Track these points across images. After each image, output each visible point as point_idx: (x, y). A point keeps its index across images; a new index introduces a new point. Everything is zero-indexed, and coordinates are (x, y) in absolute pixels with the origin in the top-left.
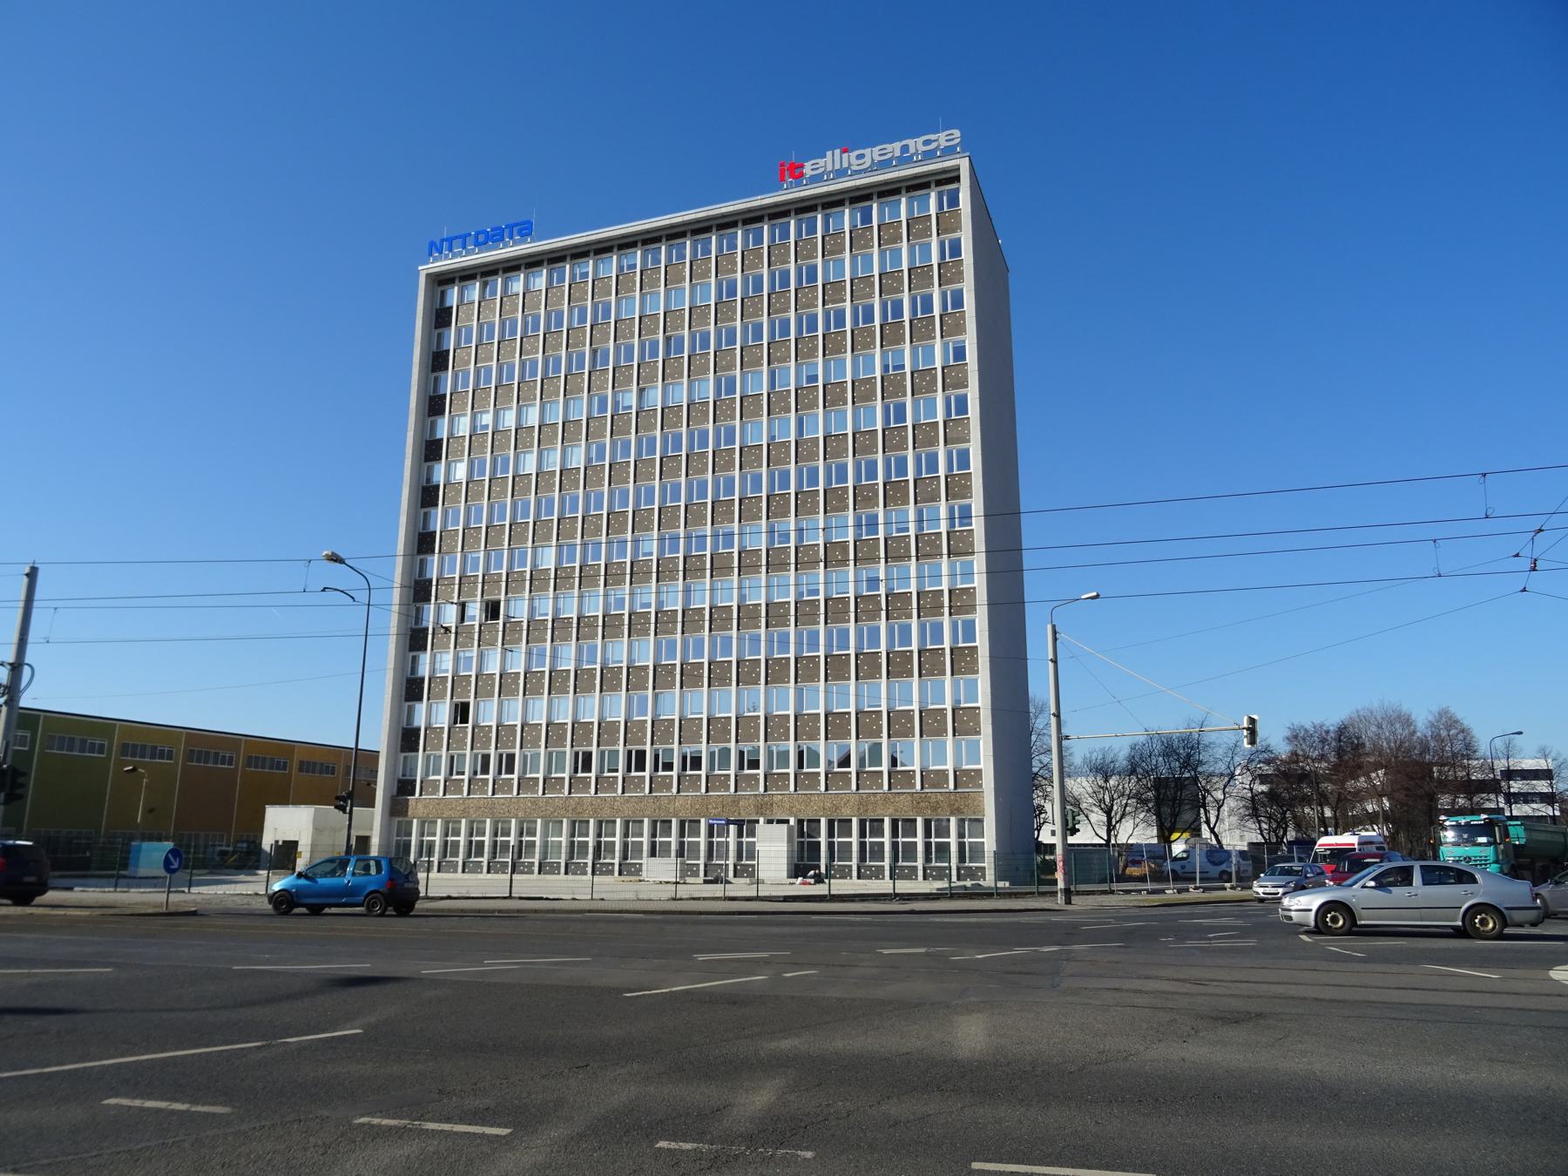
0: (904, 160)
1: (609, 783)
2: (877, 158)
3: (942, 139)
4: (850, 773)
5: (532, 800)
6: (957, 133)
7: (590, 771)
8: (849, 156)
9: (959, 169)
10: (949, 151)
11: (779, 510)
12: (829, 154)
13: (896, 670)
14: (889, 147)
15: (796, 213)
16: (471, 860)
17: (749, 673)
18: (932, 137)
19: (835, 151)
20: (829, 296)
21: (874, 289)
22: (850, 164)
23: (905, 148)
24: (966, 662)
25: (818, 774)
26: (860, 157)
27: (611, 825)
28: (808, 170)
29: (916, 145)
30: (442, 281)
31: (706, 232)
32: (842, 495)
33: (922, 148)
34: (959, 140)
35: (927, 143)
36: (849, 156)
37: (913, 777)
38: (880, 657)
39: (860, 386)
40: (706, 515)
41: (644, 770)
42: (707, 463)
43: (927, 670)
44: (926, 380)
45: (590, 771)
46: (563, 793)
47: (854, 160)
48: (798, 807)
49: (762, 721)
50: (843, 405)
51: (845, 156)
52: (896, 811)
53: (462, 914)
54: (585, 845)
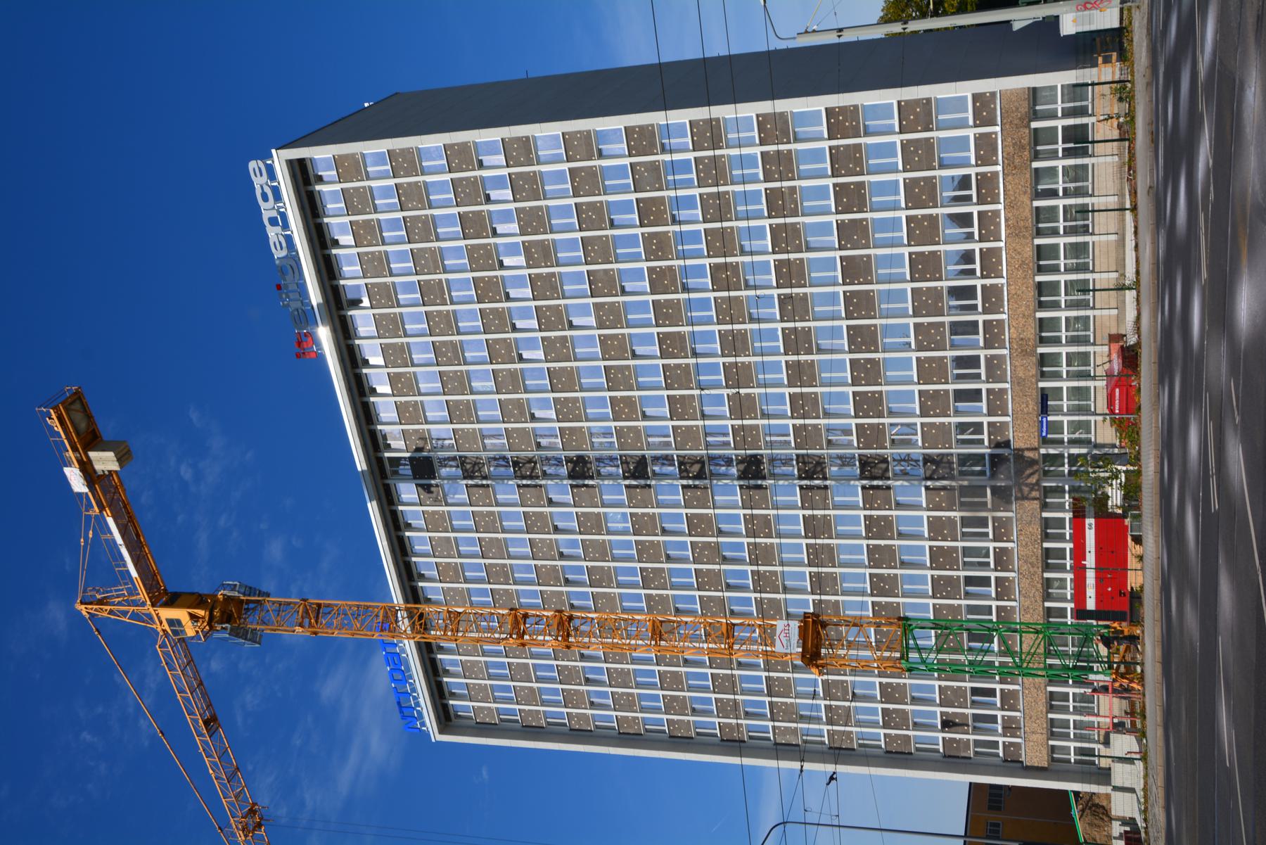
1: (1000, 527)
3: (259, 181)
5: (1022, 612)
6: (252, 165)
7: (989, 578)
10: (272, 175)
13: (857, 202)
15: (342, 308)
16: (1093, 440)
17: (867, 371)
20: (436, 298)
21: (426, 248)
23: (273, 222)
24: (845, 120)
25: (1002, 690)
29: (267, 210)
30: (446, 719)
31: (376, 437)
32: (656, 273)
34: (259, 162)
35: (265, 198)
37: (984, 175)
38: (843, 221)
40: (687, 427)
41: (977, 322)
42: (628, 428)
43: (855, 166)
45: (989, 578)
46: (1014, 578)
48: (1023, 308)
50: (555, 277)
52: (1025, 193)
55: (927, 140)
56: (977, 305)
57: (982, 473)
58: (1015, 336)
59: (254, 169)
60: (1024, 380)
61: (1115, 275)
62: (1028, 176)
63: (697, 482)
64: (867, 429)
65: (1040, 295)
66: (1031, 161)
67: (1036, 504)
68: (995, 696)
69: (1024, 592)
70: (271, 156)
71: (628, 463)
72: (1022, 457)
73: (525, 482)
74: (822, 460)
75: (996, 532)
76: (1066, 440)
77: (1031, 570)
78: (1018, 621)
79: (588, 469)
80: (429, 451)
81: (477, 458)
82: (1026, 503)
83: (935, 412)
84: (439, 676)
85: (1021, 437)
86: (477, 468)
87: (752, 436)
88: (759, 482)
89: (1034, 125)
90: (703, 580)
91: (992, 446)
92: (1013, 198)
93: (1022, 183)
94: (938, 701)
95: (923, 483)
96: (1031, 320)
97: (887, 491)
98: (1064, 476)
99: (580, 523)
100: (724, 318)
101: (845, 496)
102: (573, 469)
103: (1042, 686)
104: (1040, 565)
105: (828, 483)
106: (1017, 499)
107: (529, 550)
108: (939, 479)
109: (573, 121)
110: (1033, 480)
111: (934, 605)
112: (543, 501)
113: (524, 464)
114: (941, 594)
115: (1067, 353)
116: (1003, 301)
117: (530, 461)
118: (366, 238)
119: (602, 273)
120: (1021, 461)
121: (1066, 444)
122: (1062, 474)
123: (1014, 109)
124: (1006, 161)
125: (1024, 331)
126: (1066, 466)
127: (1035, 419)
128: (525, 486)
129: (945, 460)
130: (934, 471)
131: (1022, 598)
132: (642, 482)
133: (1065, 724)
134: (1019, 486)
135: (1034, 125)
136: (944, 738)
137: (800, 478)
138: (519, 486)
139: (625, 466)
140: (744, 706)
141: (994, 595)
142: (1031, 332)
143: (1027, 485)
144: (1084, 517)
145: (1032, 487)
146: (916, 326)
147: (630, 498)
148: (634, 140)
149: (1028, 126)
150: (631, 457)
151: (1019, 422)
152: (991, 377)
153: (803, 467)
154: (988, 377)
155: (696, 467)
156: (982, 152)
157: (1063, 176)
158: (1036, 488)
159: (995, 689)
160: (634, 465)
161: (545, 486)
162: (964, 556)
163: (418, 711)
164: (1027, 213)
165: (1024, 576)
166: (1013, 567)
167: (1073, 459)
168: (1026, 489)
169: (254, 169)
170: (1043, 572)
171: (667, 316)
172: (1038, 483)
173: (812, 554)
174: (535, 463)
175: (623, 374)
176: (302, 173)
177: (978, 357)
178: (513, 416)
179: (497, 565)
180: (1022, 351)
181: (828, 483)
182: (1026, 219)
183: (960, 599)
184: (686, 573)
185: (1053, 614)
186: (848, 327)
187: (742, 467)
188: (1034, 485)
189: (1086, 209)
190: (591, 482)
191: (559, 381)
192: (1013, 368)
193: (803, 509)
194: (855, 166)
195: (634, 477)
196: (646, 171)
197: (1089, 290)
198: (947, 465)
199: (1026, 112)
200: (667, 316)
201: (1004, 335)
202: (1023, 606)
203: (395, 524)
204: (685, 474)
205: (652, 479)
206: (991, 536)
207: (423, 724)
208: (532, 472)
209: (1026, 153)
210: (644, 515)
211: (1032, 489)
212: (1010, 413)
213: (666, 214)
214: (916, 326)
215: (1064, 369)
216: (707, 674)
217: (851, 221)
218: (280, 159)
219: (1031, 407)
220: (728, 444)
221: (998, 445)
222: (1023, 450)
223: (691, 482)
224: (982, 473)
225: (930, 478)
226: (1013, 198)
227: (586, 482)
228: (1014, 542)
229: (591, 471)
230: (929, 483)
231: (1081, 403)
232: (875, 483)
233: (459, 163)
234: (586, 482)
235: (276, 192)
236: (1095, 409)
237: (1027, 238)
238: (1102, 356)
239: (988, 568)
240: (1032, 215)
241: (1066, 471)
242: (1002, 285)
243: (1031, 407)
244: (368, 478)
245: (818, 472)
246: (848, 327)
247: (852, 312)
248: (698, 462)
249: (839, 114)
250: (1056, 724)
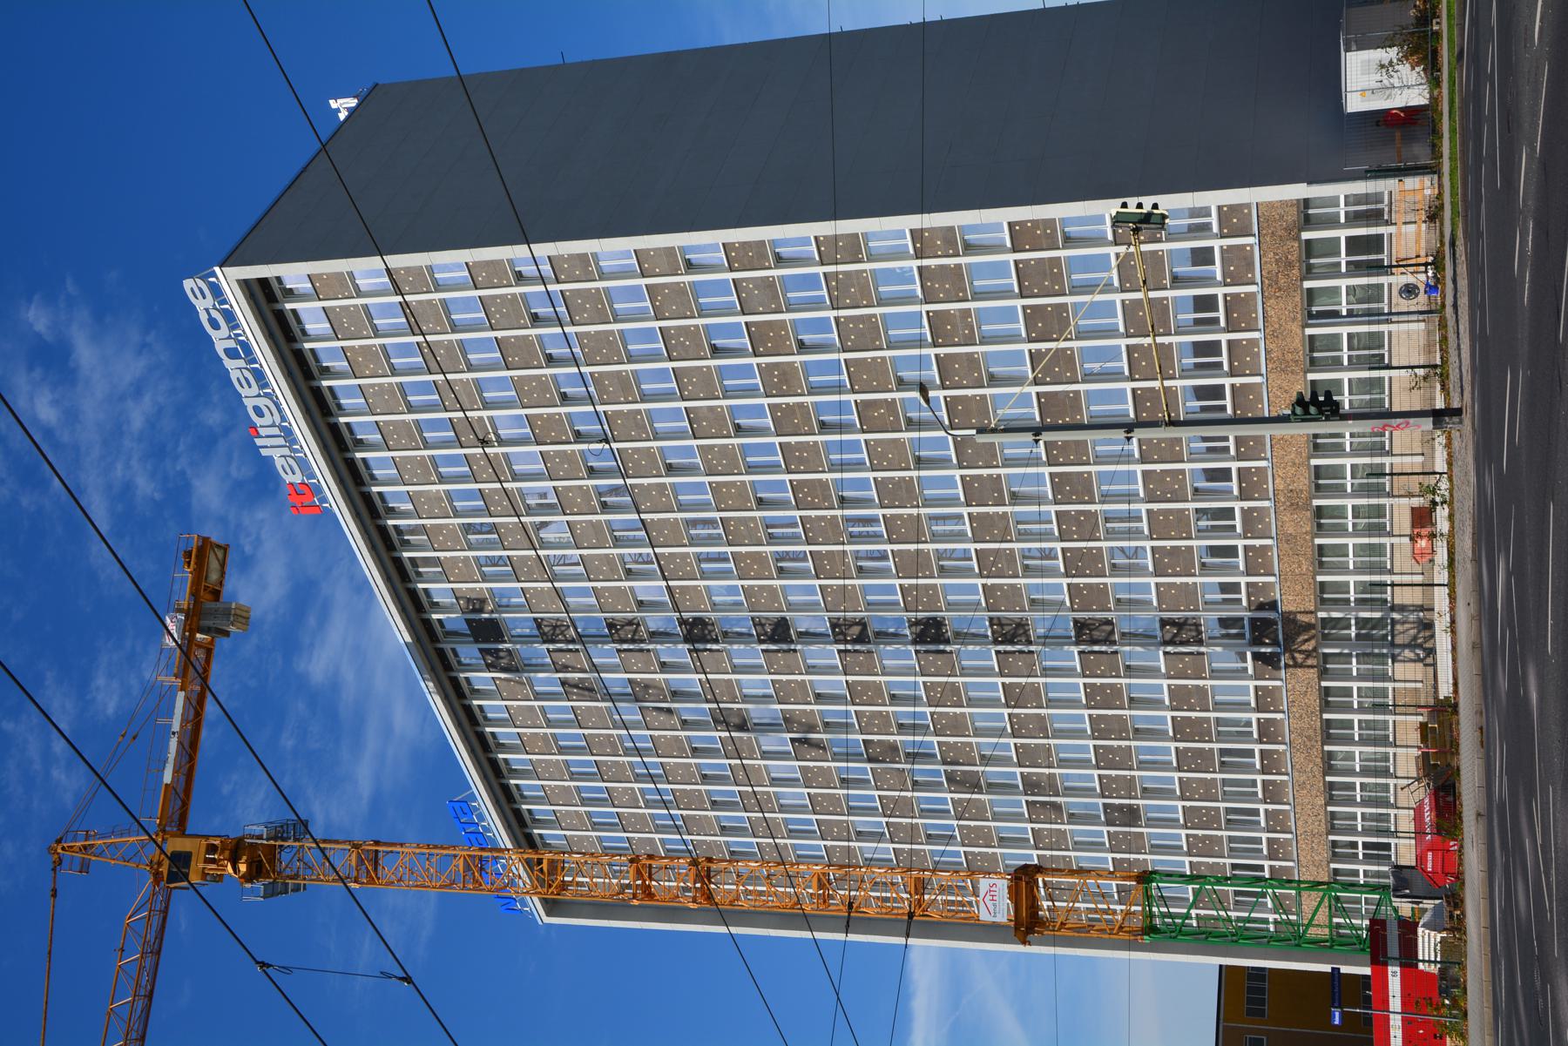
2: (255, 390)
3: (203, 305)
4: (1233, 386)
5: (1296, 788)
6: (188, 284)
7: (1229, 470)
8: (261, 426)
9: (246, 281)
10: (216, 291)
11: (819, 493)
12: (264, 452)
13: (1057, 327)
14: (234, 375)
15: (347, 450)
16: (1389, 599)
17: (1079, 524)
18: (204, 318)
19: (258, 444)
22: (273, 425)
27: (1326, 551)
28: (297, 478)
29: (221, 340)
32: (782, 410)
33: (224, 330)
34: (198, 280)
35: (215, 325)
36: (261, 426)
37: (1236, 296)
39: (608, 393)
42: (760, 587)
43: (1053, 283)
44: (583, 304)
46: (1285, 751)
47: (267, 420)
48: (1293, 456)
49: (1155, 506)
51: (262, 432)
52: (1294, 319)
53: (1479, 512)
54: (1358, 386)
56: (1210, 223)
58: (1281, 487)
59: (283, 467)
60: (1295, 537)
61: (1420, 459)
62: (1298, 299)
63: (858, 647)
66: (1302, 280)
67: (1313, 673)
69: (1298, 766)
70: (214, 274)
71: (763, 625)
72: (1294, 621)
73: (625, 646)
76: (1352, 599)
77: (1308, 743)
78: (1297, 878)
79: (710, 632)
80: (492, 612)
81: (558, 620)
82: (1299, 671)
83: (1174, 569)
84: (277, 301)
85: (1293, 600)
86: (558, 631)
87: (928, 596)
88: (942, 647)
89: (1306, 235)
91: (1253, 608)
92: (1277, 326)
93: (1290, 308)
94: (1137, 455)
95: (1162, 648)
96: (1303, 470)
98: (1351, 639)
100: (880, 463)
101: (1080, 775)
103: (1324, 863)
104: (1319, 738)
105: (1032, 648)
106: (1287, 666)
107: (543, 466)
108: (1182, 643)
109: (646, 237)
110: (1309, 646)
111: (1134, 391)
112: (654, 666)
113: (622, 626)
114: (1189, 766)
115: (1353, 506)
117: (630, 623)
118: (368, 367)
119: (706, 411)
120: (1294, 627)
121: (1352, 604)
122: (1348, 638)
123: (1277, 217)
124: (1267, 282)
125: (1294, 482)
126: (1353, 628)
127: (1311, 581)
128: (625, 650)
130: (1175, 635)
131: (1296, 774)
132: (785, 647)
133: (1337, 472)
135: (1306, 235)
136: (1180, 779)
137: (996, 642)
138: (619, 651)
139: (759, 628)
140: (865, 594)
141: (1236, 492)
142: (1304, 482)
143: (1300, 652)
144: (1386, 965)
145: (1308, 654)
146: (1144, 473)
147: (770, 664)
149: (1298, 238)
150: (767, 619)
151: (1288, 584)
152: (1231, 279)
153: (999, 629)
154: (1245, 531)
155: (856, 630)
156: (1232, 268)
157: (1348, 294)
158: (1314, 654)
159: (1212, 248)
160: (772, 627)
161: (655, 651)
162: (1230, 842)
163: (483, 827)
164: (1297, 343)
165: (1298, 750)
166: (1284, 738)
167: (1362, 623)
169: (283, 467)
170: (1323, 745)
171: (801, 460)
172: (1315, 649)
174: (638, 625)
175: (747, 526)
176: (264, 296)
177: (1216, 296)
178: (602, 572)
179: (599, 736)
180: (1292, 504)
181: (1032, 648)
182: (1296, 351)
183: (1214, 772)
184: (746, 371)
185: (1327, 589)
186: (1051, 474)
189: (1380, 264)
190: (715, 647)
191: (660, 533)
193: (935, 346)
194: (1053, 283)
195: (772, 640)
196: (756, 287)
197: (1386, 474)
198: (1193, 628)
199: (1294, 221)
200: (801, 460)
201: (1267, 484)
204: (841, 637)
205: (798, 643)
206: (1223, 323)
207: (325, 500)
208: (634, 635)
209: (1296, 272)
210: (789, 682)
211: (1307, 657)
212: (1263, 371)
213: (790, 340)
214: (1144, 473)
215: (1350, 522)
216: (785, 481)
218: (229, 278)
219: (1304, 567)
220: (820, 301)
221: (1261, 607)
222: (1295, 613)
223: (849, 647)
225: (1171, 642)
226: (1277, 326)
227: (709, 646)
228: (1284, 712)
229: (713, 634)
230: (1169, 649)
231: (1373, 559)
232: (1096, 648)
233: (487, 276)
234: (709, 646)
235: (229, 316)
237: (1297, 374)
238: (1407, 726)
239: (1208, 233)
240: (1303, 346)
241: (1353, 635)
242: (1251, 246)
243: (1304, 567)
245: (1020, 635)
246: (1051, 474)
247: (1057, 457)
250: (1322, 472)
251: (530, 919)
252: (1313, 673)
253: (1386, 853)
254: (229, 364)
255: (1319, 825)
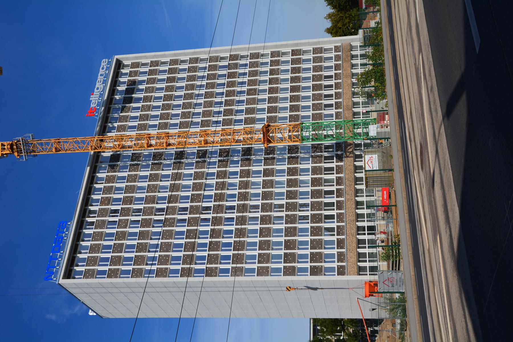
0: (107, 76)
1: (338, 169)
10: (109, 63)
17: (295, 118)
23: (101, 75)
26: (98, 89)
35: (103, 68)
37: (337, 64)
38: (293, 77)
55: (320, 253)
57: (333, 151)
64: (295, 51)
65: (359, 257)
67: (352, 159)
68: (334, 219)
74: (274, 149)
75: (337, 171)
77: (350, 183)
82: (348, 158)
85: (347, 136)
90: (217, 198)
97: (297, 159)
99: (163, 233)
101: (280, 173)
102: (177, 156)
106: (345, 157)
110: (351, 150)
116: (341, 96)
129: (319, 147)
134: (345, 152)
142: (350, 104)
143: (348, 152)
145: (350, 153)
148: (232, 58)
158: (352, 153)
165: (347, 186)
168: (348, 154)
172: (352, 151)
173: (264, 184)
185: (354, 75)
187: (243, 153)
188: (351, 152)
192: (344, 114)
202: (347, 198)
203: (92, 179)
209: (349, 58)
211: (350, 153)
217: (295, 76)
224: (333, 151)
236: (380, 269)
244: (92, 157)
248: (226, 152)
249: (295, 51)
251: (16, 157)
252: (352, 159)
253: (374, 232)
254: (99, 77)
255: (353, 217)
